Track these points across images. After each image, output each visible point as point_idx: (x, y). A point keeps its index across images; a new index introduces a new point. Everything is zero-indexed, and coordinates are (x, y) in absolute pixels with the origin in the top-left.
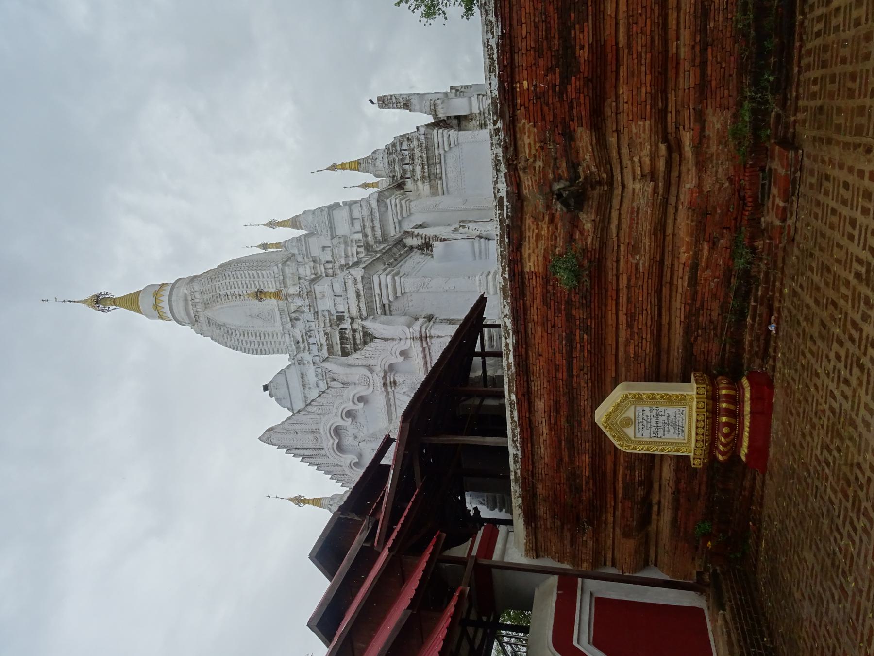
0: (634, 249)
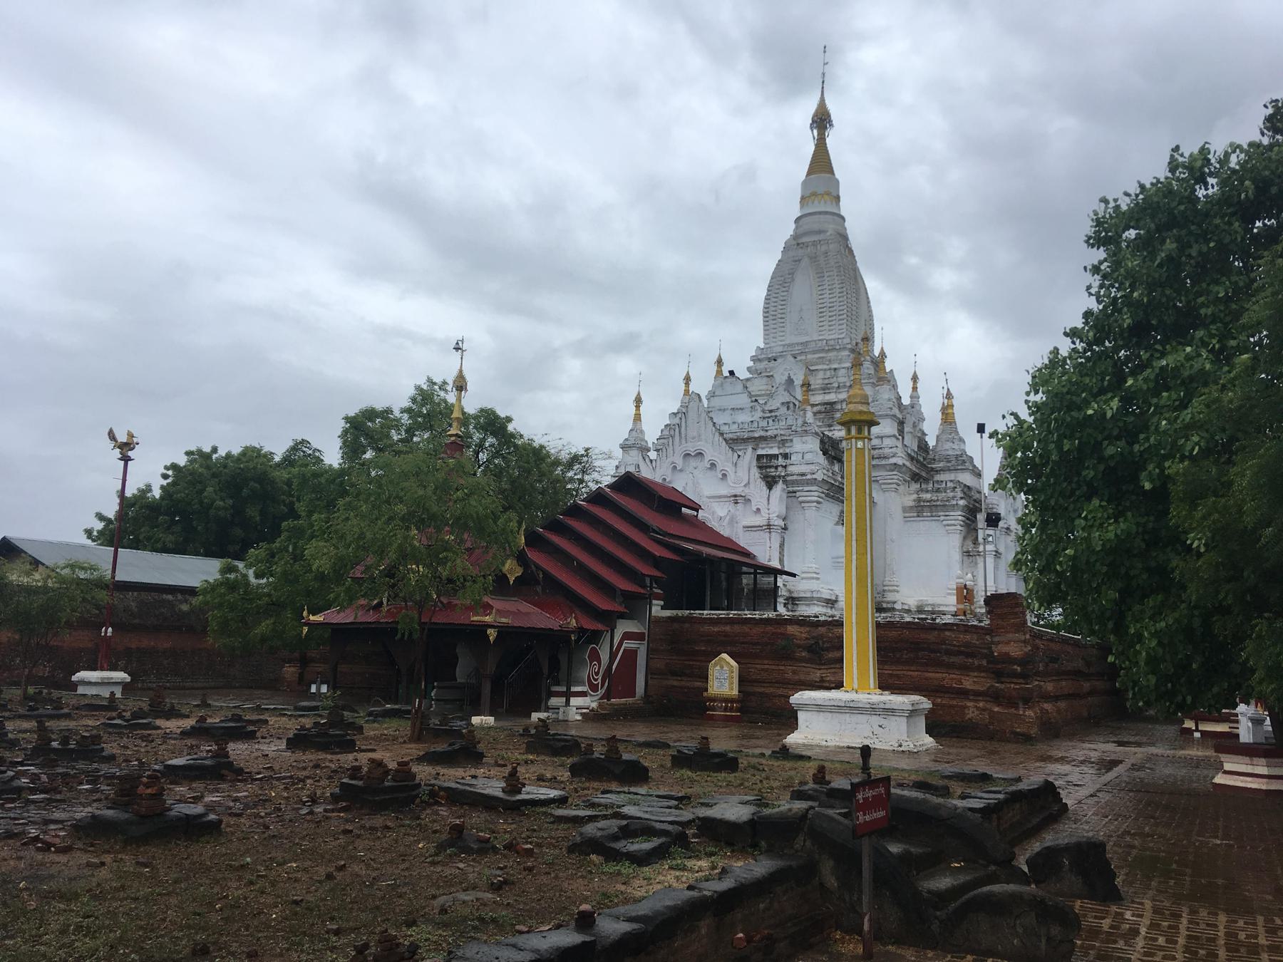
0: (794, 672)
